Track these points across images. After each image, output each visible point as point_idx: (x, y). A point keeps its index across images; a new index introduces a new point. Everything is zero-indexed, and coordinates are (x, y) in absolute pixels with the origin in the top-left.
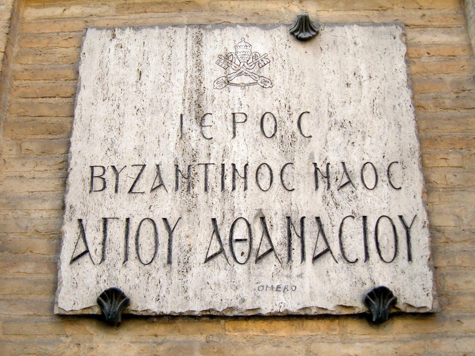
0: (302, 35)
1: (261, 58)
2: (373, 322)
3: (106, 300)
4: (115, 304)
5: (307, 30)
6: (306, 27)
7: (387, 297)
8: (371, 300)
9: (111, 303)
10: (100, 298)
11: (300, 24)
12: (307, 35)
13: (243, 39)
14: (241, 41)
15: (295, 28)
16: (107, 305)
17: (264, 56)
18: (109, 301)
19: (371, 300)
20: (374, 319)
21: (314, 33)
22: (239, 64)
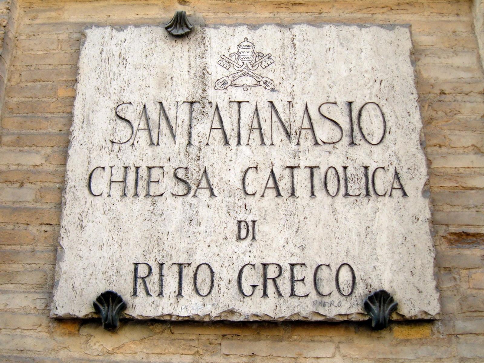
0: (175, 32)
1: (264, 58)
2: (372, 327)
3: (102, 304)
4: (112, 308)
5: (181, 26)
6: (180, 23)
7: (387, 302)
8: (370, 304)
9: (380, 307)
10: (97, 303)
11: (174, 21)
12: (180, 32)
13: (246, 39)
14: (244, 41)
15: (170, 23)
16: (375, 308)
17: (267, 57)
18: (377, 304)
19: (370, 304)
20: (373, 325)
21: (187, 30)
22: (241, 64)
